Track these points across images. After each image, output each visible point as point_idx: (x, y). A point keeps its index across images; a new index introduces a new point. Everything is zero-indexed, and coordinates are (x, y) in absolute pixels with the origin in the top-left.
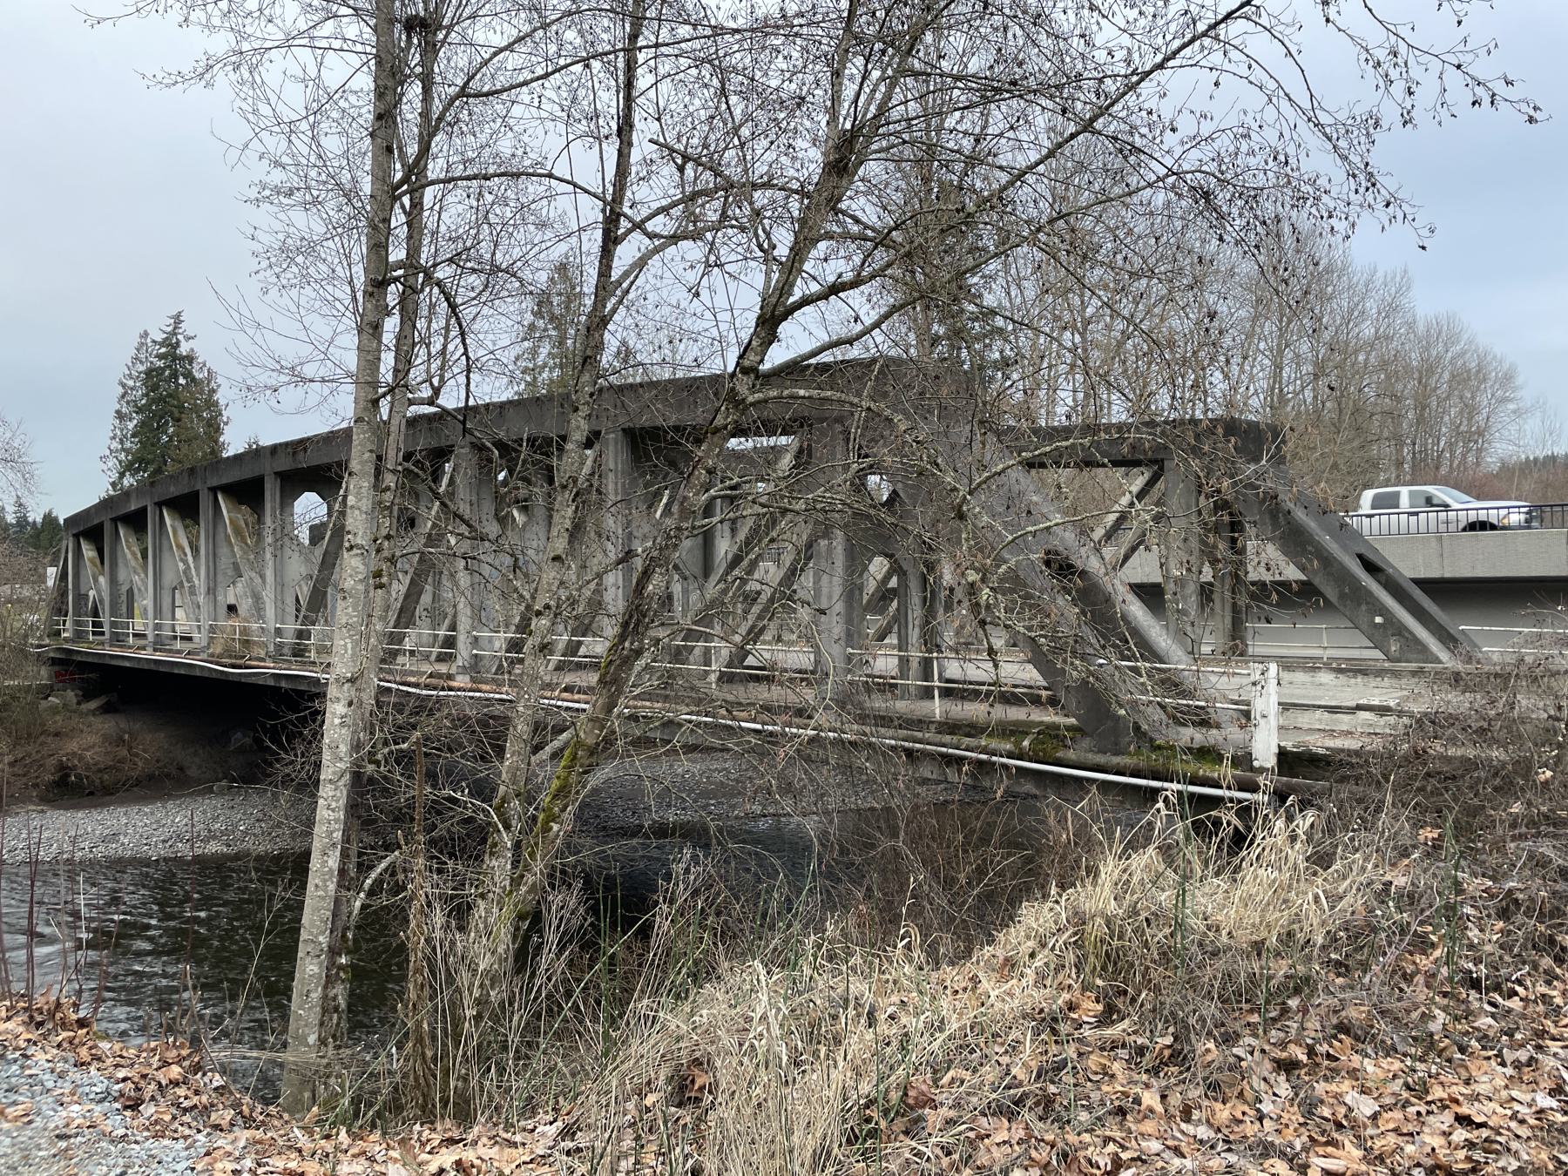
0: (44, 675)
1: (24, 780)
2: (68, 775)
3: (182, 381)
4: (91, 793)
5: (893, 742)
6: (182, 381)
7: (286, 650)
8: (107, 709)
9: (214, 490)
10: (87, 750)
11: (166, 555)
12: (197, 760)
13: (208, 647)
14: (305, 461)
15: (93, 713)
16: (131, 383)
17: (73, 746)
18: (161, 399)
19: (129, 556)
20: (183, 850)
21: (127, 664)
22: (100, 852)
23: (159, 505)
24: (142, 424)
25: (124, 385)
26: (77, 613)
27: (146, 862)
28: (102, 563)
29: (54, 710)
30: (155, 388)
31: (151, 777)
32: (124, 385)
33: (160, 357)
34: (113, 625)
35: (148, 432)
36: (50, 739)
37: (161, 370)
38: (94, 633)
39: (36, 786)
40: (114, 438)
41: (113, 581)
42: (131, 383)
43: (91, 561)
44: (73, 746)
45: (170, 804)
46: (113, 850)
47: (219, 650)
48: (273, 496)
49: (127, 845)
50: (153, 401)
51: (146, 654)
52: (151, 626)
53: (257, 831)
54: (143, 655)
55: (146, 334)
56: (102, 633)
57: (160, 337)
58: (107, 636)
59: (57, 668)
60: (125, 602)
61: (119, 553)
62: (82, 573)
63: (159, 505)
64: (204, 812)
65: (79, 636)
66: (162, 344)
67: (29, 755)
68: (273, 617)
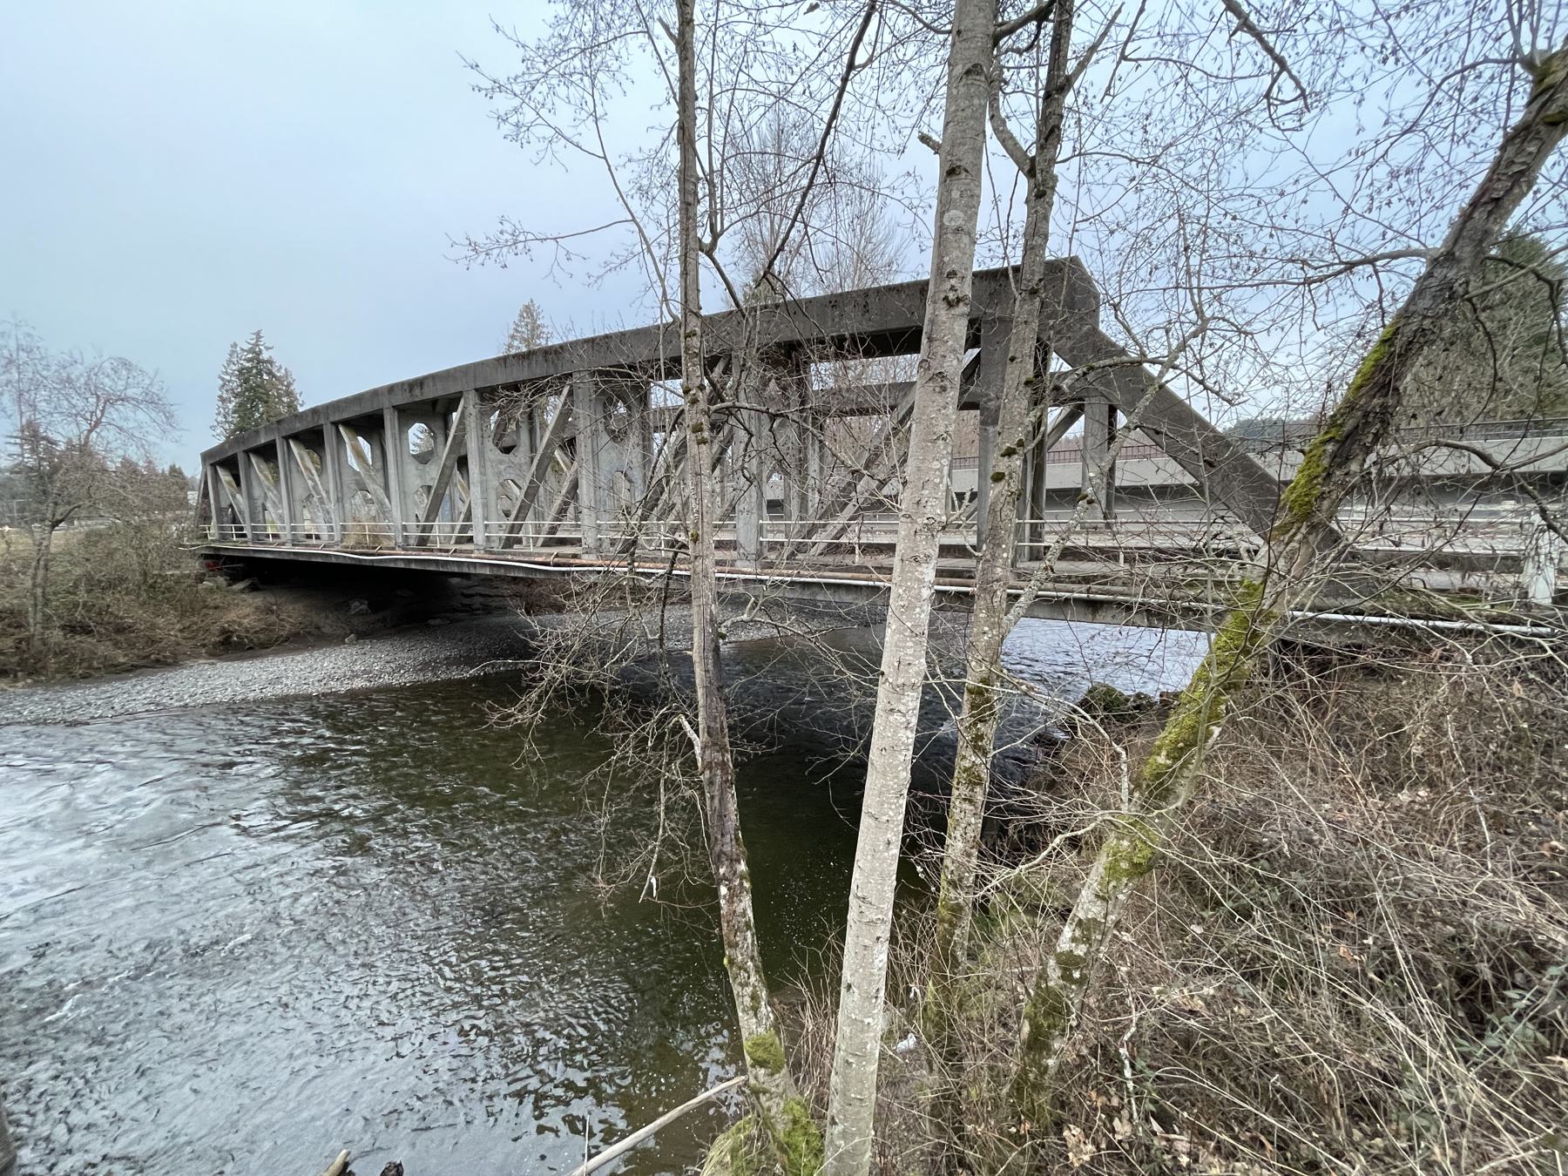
0: (195, 566)
1: (194, 642)
2: (230, 637)
3: (265, 377)
4: (251, 648)
5: (1340, 617)
6: (265, 377)
7: (412, 541)
8: (253, 588)
9: (335, 424)
10: (244, 618)
11: (295, 475)
12: (329, 621)
13: (342, 541)
14: (419, 395)
15: (242, 591)
16: (228, 378)
17: (232, 616)
18: (250, 389)
19: (262, 478)
20: (335, 686)
21: (320, 560)
22: (269, 692)
23: (287, 438)
24: (240, 405)
25: (223, 379)
26: (220, 521)
27: (309, 697)
28: (238, 484)
29: (211, 591)
30: (246, 381)
31: (297, 635)
32: (223, 379)
33: (249, 360)
34: (254, 528)
35: (244, 410)
36: (211, 612)
37: (249, 370)
38: (238, 536)
39: (204, 646)
40: (219, 414)
41: (250, 497)
42: (228, 378)
43: (229, 483)
44: (232, 616)
45: (316, 654)
46: (279, 690)
47: (352, 543)
48: (393, 427)
49: (289, 686)
50: (247, 390)
51: (288, 548)
52: (288, 528)
53: (389, 670)
54: (283, 549)
55: (235, 345)
56: (244, 536)
57: (247, 347)
58: (249, 536)
59: (210, 561)
60: (257, 511)
61: (253, 477)
62: (221, 492)
63: (287, 438)
64: (344, 658)
65: (224, 538)
66: (249, 351)
67: (196, 623)
68: (399, 517)
